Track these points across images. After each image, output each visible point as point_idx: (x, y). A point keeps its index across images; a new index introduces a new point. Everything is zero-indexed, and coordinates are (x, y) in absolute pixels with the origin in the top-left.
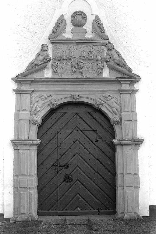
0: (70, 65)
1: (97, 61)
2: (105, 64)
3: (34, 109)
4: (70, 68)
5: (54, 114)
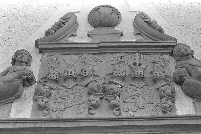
0: (85, 90)
2: (178, 89)
4: (85, 98)
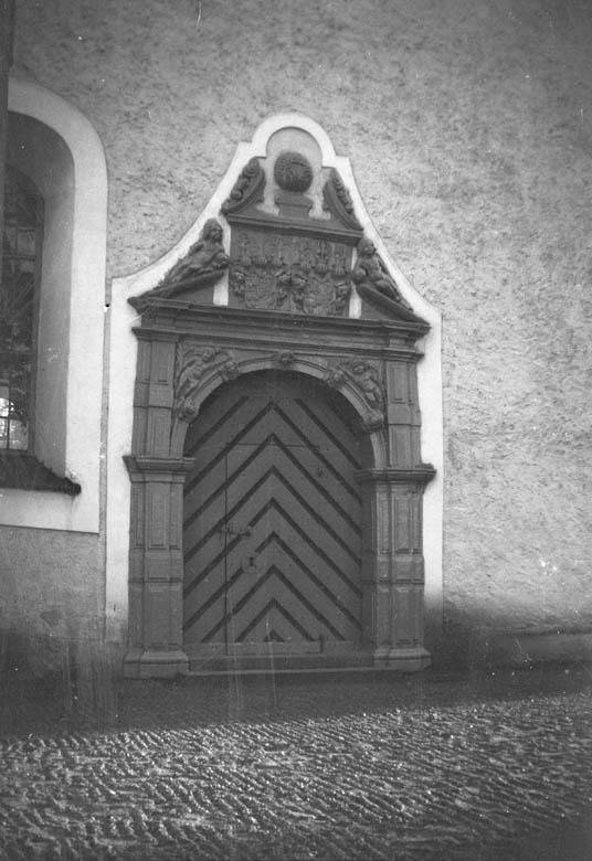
3: (183, 378)
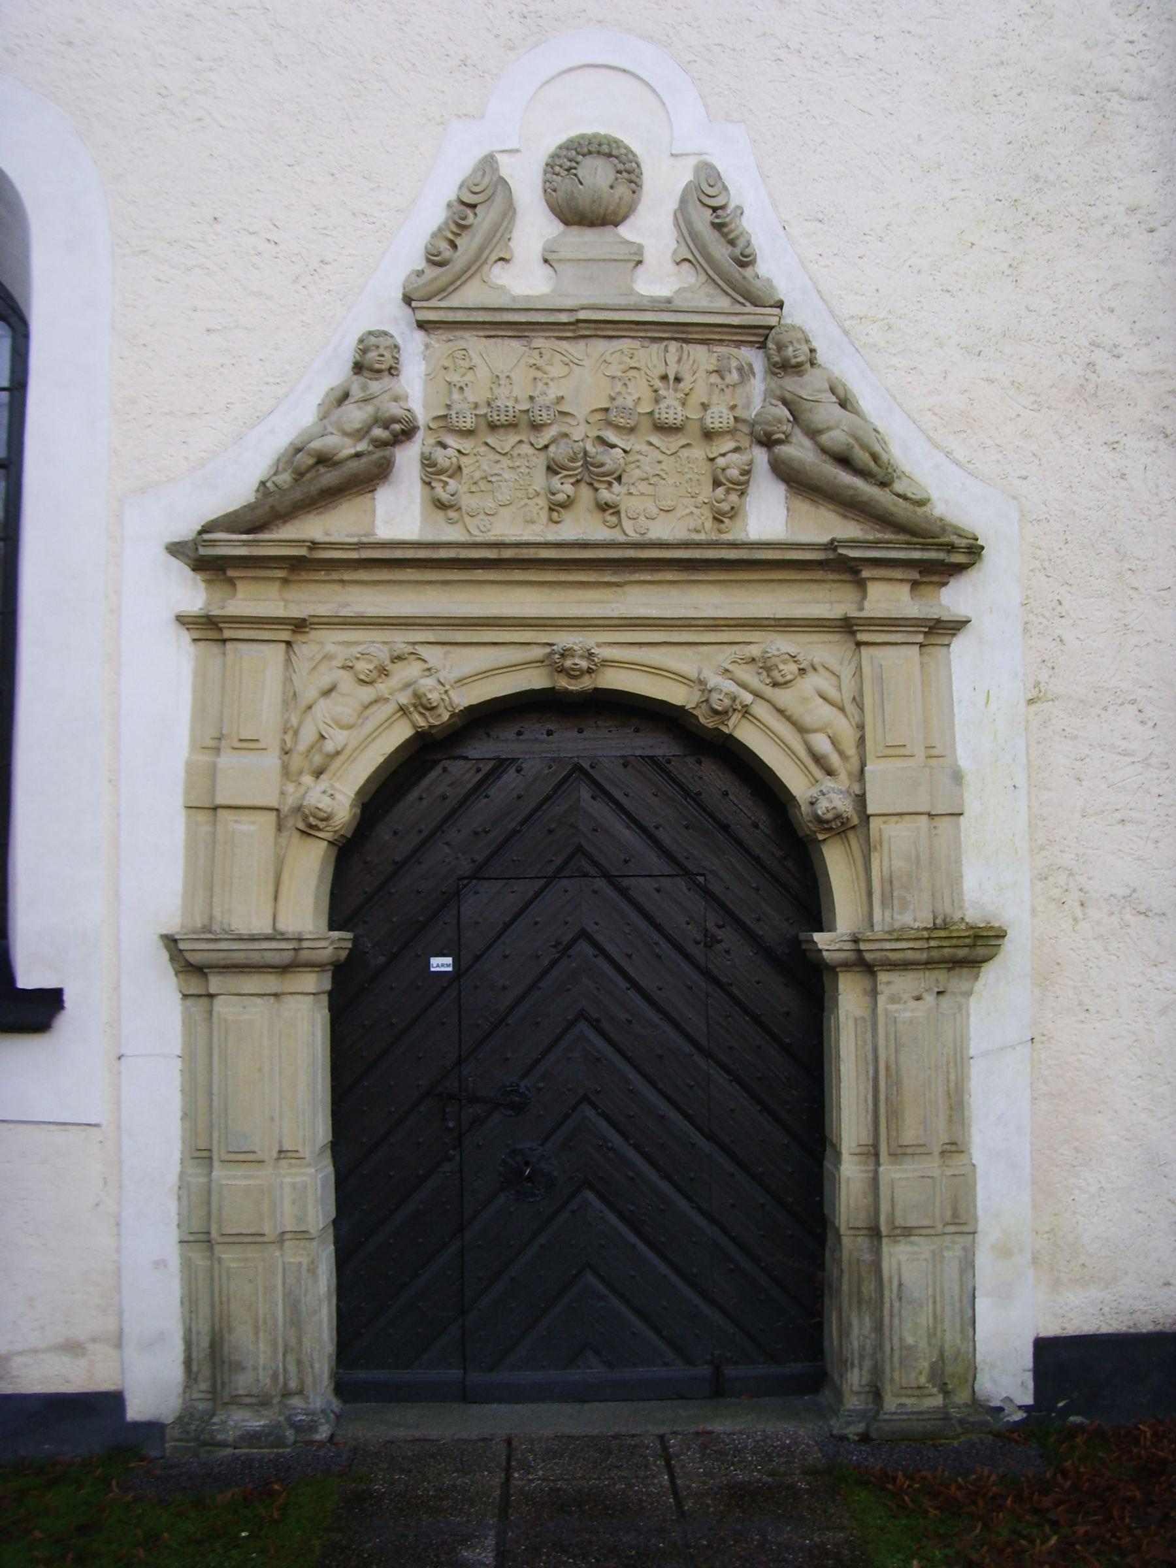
0: (540, 461)
1: (709, 435)
2: (760, 456)
3: (308, 734)
4: (539, 479)
5: (437, 771)
